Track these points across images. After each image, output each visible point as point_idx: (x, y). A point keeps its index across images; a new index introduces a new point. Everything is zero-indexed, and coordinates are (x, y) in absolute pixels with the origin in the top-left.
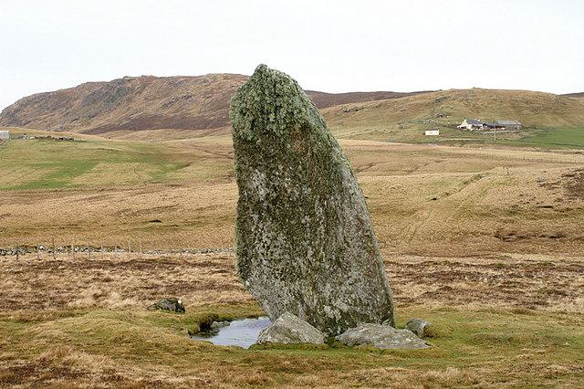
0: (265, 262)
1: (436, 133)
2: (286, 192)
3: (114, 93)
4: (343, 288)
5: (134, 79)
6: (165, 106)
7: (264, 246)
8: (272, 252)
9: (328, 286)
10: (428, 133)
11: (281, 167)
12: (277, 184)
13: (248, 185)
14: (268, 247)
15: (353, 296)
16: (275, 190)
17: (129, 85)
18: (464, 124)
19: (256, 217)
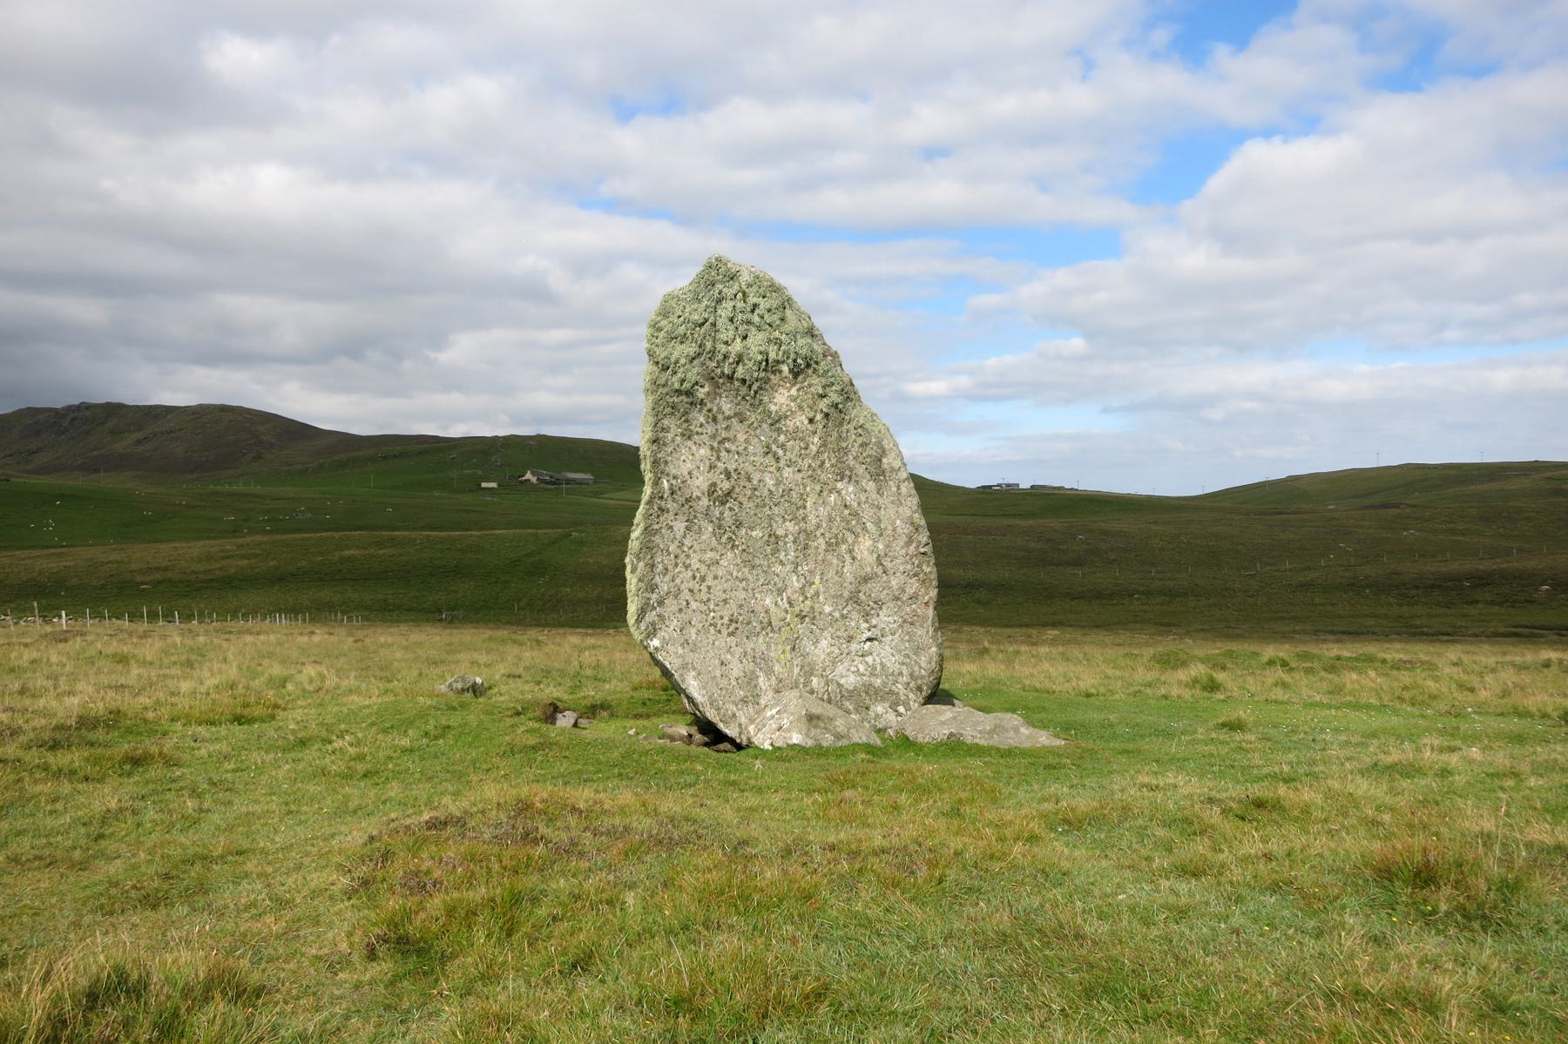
0: (694, 605)
1: (493, 485)
2: (749, 479)
3: (65, 423)
4: (854, 646)
5: (96, 406)
6: (138, 442)
7: (694, 577)
8: (709, 588)
9: (824, 643)
10: (484, 485)
11: (741, 437)
12: (731, 467)
13: (672, 470)
14: (703, 579)
15: (869, 659)
16: (728, 476)
17: (88, 413)
18: (528, 476)
19: (680, 526)
